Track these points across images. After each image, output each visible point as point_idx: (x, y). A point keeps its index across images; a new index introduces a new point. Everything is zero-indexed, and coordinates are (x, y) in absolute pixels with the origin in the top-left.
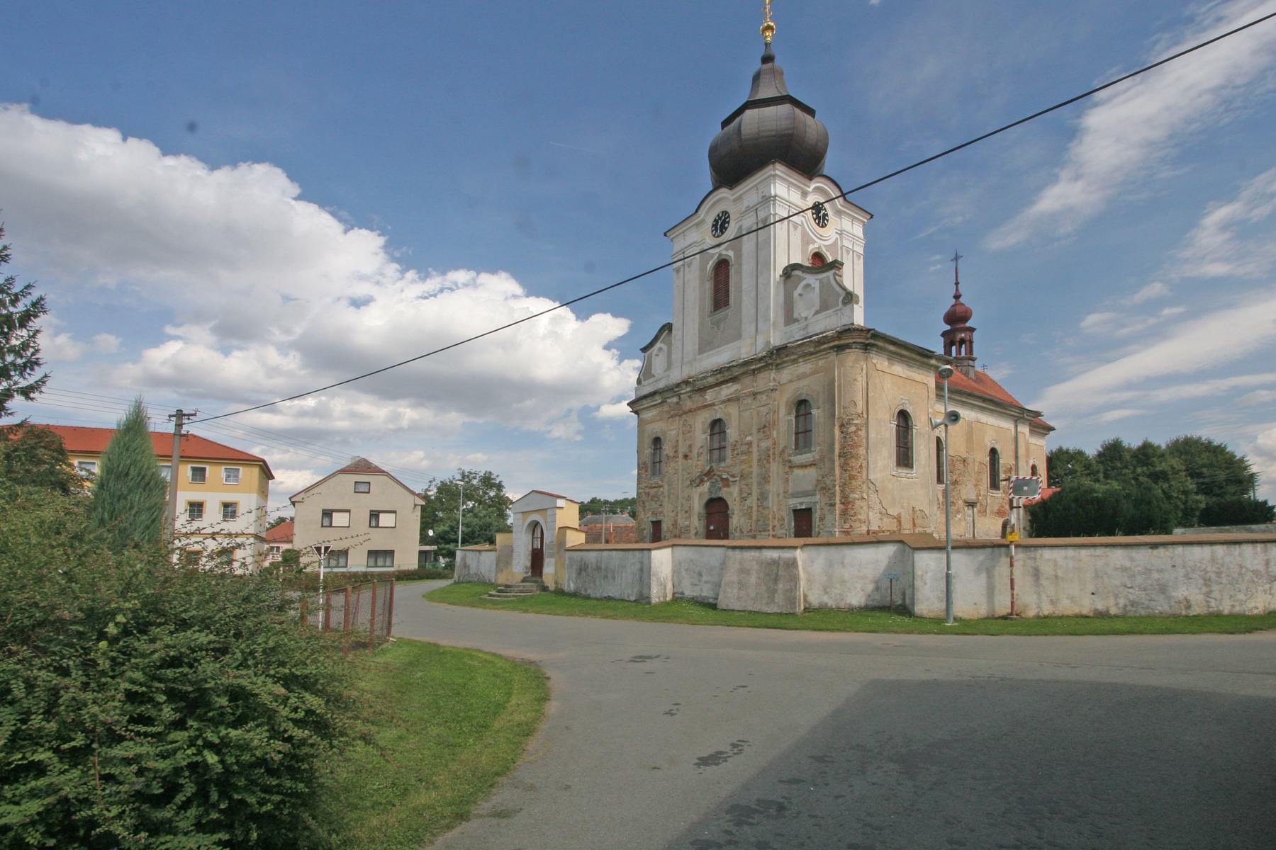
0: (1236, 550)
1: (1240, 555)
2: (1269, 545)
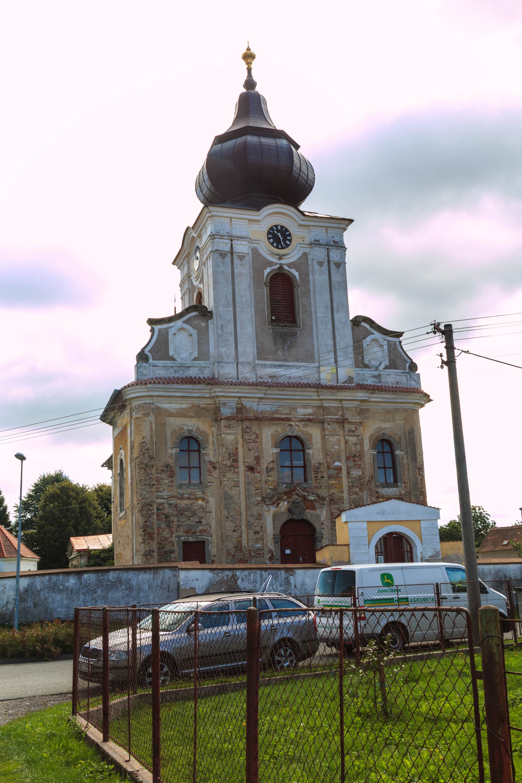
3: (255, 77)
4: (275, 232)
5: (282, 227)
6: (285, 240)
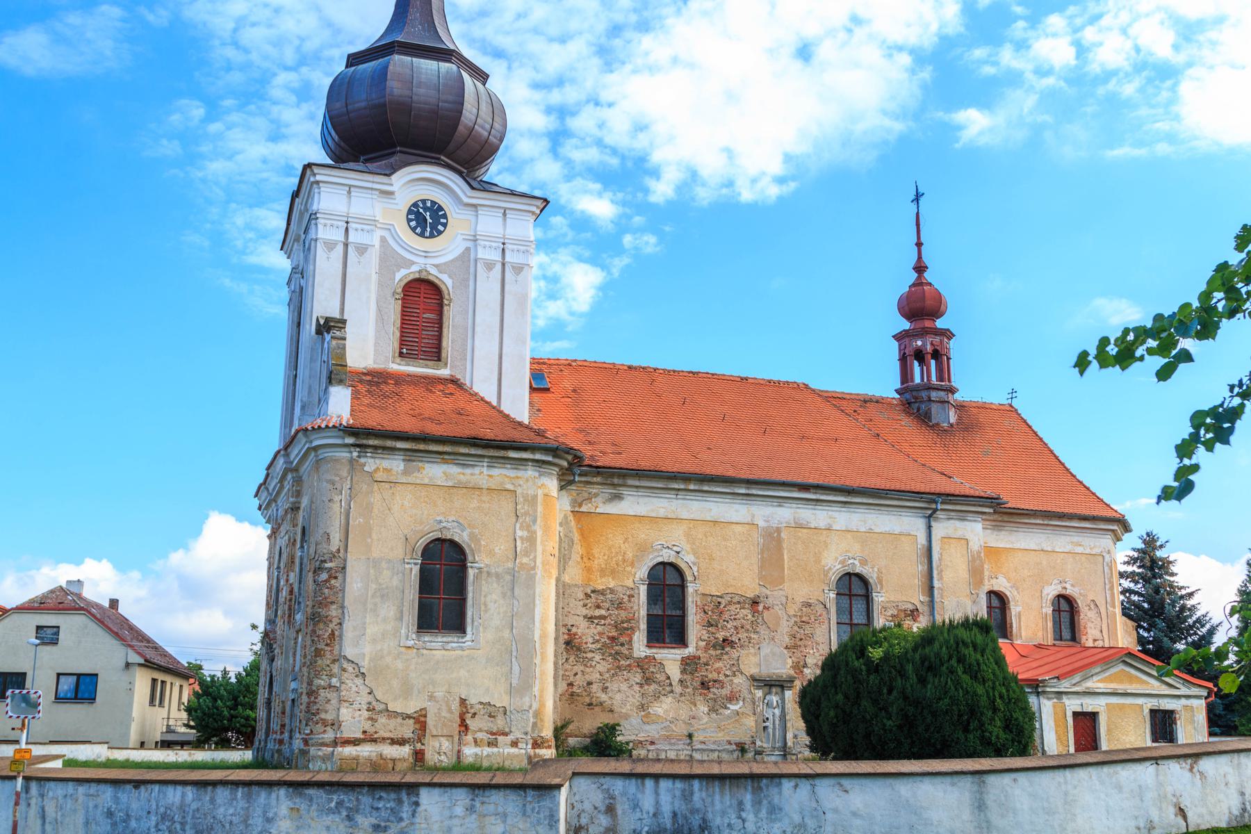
0: (208, 794)
1: (212, 801)
2: (255, 789)
5: (434, 203)
6: (434, 227)
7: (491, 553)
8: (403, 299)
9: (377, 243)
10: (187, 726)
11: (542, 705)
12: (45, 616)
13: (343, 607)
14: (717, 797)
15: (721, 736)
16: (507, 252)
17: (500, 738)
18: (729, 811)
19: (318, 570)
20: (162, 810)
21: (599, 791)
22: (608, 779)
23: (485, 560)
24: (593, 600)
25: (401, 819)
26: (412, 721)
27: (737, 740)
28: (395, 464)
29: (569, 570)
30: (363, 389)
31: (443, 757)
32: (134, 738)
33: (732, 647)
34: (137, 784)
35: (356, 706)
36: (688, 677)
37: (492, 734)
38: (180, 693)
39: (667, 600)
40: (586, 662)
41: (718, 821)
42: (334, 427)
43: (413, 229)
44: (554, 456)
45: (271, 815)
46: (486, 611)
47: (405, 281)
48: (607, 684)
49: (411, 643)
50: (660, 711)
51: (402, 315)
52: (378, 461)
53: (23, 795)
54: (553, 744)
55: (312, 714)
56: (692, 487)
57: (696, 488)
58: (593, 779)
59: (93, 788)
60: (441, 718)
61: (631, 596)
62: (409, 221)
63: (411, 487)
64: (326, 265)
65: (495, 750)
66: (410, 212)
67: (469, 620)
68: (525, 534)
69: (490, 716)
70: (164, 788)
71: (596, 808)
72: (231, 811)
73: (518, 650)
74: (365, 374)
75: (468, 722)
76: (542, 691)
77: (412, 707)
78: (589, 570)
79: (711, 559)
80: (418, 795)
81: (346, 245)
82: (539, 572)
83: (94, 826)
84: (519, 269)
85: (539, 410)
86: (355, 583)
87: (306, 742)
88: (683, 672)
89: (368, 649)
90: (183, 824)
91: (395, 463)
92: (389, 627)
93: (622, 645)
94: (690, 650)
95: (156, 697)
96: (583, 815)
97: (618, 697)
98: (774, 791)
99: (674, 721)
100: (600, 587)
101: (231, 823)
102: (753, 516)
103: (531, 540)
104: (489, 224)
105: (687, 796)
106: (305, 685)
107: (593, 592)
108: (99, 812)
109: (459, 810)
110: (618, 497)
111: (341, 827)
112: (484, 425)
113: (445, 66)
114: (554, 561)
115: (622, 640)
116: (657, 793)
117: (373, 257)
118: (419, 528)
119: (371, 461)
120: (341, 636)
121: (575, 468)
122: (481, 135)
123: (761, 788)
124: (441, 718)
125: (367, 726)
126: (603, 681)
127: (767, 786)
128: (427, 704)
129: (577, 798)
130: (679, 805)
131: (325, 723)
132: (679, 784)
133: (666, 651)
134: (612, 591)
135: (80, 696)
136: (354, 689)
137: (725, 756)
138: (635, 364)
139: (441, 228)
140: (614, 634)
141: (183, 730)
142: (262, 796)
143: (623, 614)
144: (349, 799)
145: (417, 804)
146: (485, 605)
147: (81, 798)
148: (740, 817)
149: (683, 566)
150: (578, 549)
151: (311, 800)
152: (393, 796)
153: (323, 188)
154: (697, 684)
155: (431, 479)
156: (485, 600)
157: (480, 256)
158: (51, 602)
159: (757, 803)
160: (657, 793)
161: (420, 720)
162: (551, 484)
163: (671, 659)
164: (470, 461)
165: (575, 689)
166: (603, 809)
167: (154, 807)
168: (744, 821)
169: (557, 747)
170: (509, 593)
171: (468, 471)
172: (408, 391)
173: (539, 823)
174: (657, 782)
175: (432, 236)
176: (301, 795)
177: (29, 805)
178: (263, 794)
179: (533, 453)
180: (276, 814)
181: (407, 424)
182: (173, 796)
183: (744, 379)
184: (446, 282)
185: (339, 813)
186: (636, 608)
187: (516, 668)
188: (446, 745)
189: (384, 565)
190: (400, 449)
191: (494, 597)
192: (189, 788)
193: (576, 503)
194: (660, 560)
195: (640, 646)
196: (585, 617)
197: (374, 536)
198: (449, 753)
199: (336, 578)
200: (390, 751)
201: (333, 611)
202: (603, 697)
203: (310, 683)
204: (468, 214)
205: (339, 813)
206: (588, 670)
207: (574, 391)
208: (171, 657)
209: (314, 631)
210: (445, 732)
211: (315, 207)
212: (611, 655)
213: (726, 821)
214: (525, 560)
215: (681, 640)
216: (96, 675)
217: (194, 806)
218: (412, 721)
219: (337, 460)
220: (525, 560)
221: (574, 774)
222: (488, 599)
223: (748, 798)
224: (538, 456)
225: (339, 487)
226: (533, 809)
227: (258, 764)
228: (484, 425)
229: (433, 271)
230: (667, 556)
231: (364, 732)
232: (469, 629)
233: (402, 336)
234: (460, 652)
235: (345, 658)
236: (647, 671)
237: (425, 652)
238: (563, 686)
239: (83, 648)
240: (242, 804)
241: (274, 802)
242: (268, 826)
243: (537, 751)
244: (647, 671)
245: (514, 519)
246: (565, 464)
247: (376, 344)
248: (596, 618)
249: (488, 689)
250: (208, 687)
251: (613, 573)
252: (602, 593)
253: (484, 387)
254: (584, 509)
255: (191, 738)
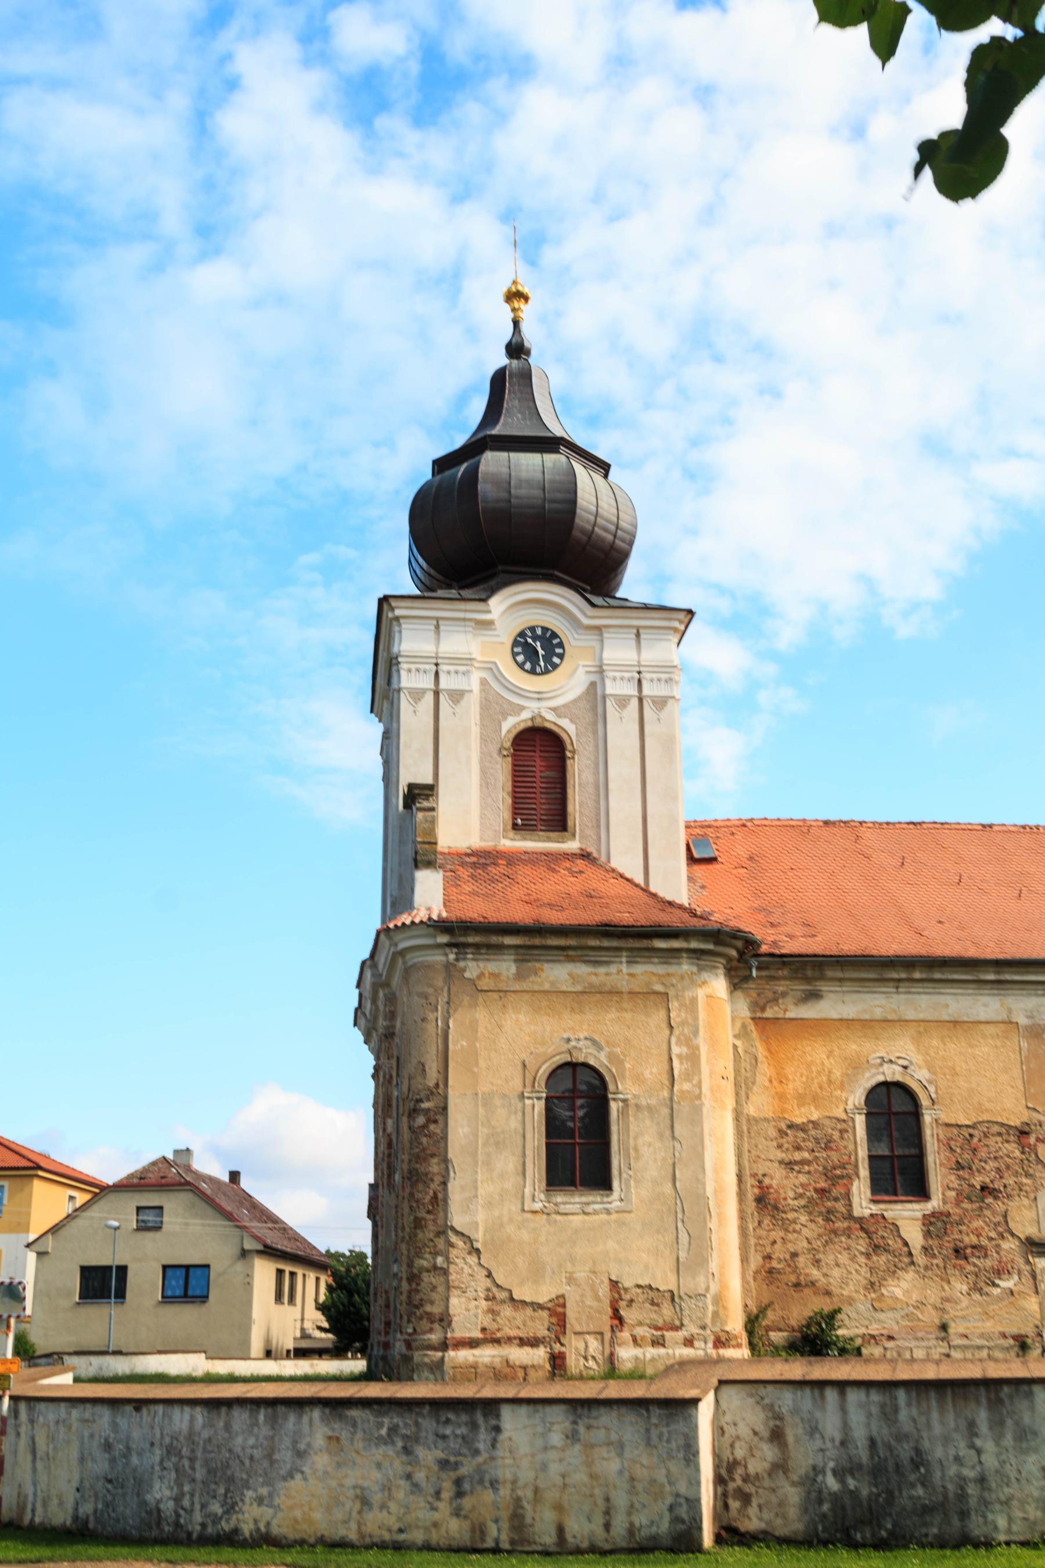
1: (228, 1427)
2: (281, 1409)
3: (530, 335)
4: (530, 640)
5: (545, 629)
6: (548, 659)
7: (639, 1079)
8: (514, 756)
9: (475, 686)
10: (321, 1329)
11: (724, 1286)
12: (147, 1195)
13: (446, 1161)
14: (935, 1415)
15: (990, 1326)
16: (645, 683)
17: (668, 1335)
18: (956, 1436)
19: (414, 1112)
20: (167, 1440)
21: (758, 1409)
22: (770, 1388)
23: (632, 1087)
24: (791, 1139)
25: (477, 1452)
26: (545, 1314)
27: (1015, 1331)
28: (506, 967)
29: (753, 1098)
30: (464, 873)
31: (591, 1363)
32: (257, 1346)
33: (996, 1198)
34: (139, 1404)
35: (471, 1294)
36: (934, 1243)
37: (657, 1328)
38: (313, 1287)
39: (895, 1134)
40: (786, 1226)
41: (939, 1452)
42: (422, 922)
43: (521, 666)
44: (716, 944)
45: (302, 1446)
46: (637, 1158)
47: (515, 732)
48: (821, 1256)
49: (538, 1206)
50: (898, 1292)
51: (514, 776)
52: (481, 964)
53: (11, 1422)
54: (744, 1339)
55: (414, 1305)
56: (917, 975)
57: (924, 976)
58: (747, 1387)
59: (88, 1411)
60: (586, 1309)
61: (842, 1132)
62: (514, 655)
63: (527, 997)
64: (414, 719)
65: (662, 1351)
66: (516, 643)
67: (615, 1172)
68: (684, 1050)
69: (653, 1303)
70: (169, 1409)
71: (755, 1433)
72: (251, 1441)
73: (685, 1210)
74: (467, 855)
75: (622, 1313)
76: (722, 1267)
77: (544, 1294)
78: (782, 1097)
79: (955, 1074)
80: (498, 1416)
81: (437, 693)
82: (707, 1101)
83: (90, 1464)
84: (661, 703)
85: (703, 887)
86: (460, 1129)
87: (409, 1345)
88: (927, 1234)
89: (481, 1217)
90: (192, 1460)
91: (504, 965)
92: (509, 1185)
93: (836, 1199)
94: (934, 1204)
95: (284, 1292)
96: (737, 1445)
97: (836, 1273)
98: (1022, 1405)
99: (921, 1305)
100: (799, 1121)
101: (252, 1458)
102: (1010, 1011)
103: (693, 1058)
104: (618, 651)
105: (889, 1414)
106: (404, 1268)
107: (789, 1127)
108: (95, 1444)
109: (556, 1438)
110: (815, 996)
111: (397, 1463)
112: (622, 908)
113: (550, 458)
114: (729, 1087)
115: (835, 1192)
116: (843, 1410)
117: (472, 705)
118: (541, 1050)
119: (471, 964)
120: (445, 1200)
121: (742, 956)
122: (603, 540)
123: (1000, 1401)
124: (586, 1309)
125: (487, 1321)
126: (812, 1250)
127: (1011, 1397)
128: (566, 1289)
129: (728, 1418)
130: (881, 1431)
131: (430, 1317)
132: (875, 1397)
133: (899, 1206)
134: (815, 1124)
135: (190, 1293)
136: (467, 1270)
137: (998, 1354)
138: (833, 818)
139: (556, 660)
140: (822, 1184)
141: (318, 1334)
142: (291, 1420)
143: (834, 1156)
144: (404, 1422)
145: (497, 1429)
146: (636, 1150)
147: (75, 1425)
148: (972, 1446)
149: (914, 1086)
150: (765, 1070)
151: (354, 1425)
152: (464, 1418)
153: (405, 625)
154: (948, 1251)
155: (552, 983)
156: (637, 1144)
157: (608, 691)
158: (152, 1178)
159: (997, 1424)
160: (843, 1410)
161: (557, 1313)
162: (718, 985)
163: (908, 1217)
164: (604, 957)
165: (775, 1264)
166: (766, 1433)
167: (158, 1436)
168: (979, 1452)
169: (752, 1346)
170: (668, 1133)
171: (602, 970)
172: (524, 873)
173: (670, 1456)
174: (842, 1394)
175: (546, 672)
176: (341, 1417)
177: (18, 1434)
178: (292, 1418)
179: (687, 940)
180: (309, 1445)
181: (520, 914)
182: (181, 1420)
183: (987, 827)
184: (568, 727)
185: (393, 1443)
186: (851, 1147)
187: (684, 1238)
188: (594, 1344)
189: (498, 1102)
190: (510, 947)
191: (648, 1138)
192: (198, 1409)
193: (758, 1006)
194: (881, 1078)
195: (862, 1198)
196: (781, 1162)
197: (482, 1063)
198: (599, 1357)
199: (436, 1122)
200: (520, 1355)
201: (434, 1167)
202: (815, 1274)
203: (410, 1265)
204: (590, 640)
205: (393, 1443)
206: (790, 1236)
207: (751, 858)
208: (304, 1241)
209: (412, 1195)
210: (592, 1328)
211: (395, 650)
212: (820, 1214)
213: (952, 1452)
214: (686, 1086)
215: (920, 1190)
216: (208, 1266)
217: (206, 1434)
218: (545, 1314)
219: (429, 967)
220: (686, 1086)
221: (721, 1382)
222: (640, 1141)
223: (982, 1416)
224: (694, 944)
225: (433, 1002)
226: (660, 1437)
227: (368, 1377)
228: (622, 908)
229: (550, 716)
230: (892, 1073)
231: (484, 1330)
232: (616, 1184)
233: (514, 803)
234: (604, 1217)
235: (453, 1229)
236: (876, 1236)
237: (558, 1218)
238: (756, 1260)
239: (189, 1234)
240: (265, 1431)
241: (306, 1428)
242: (298, 1461)
243: (722, 1351)
244: (876, 1236)
245: (668, 1032)
246: (734, 953)
247: (483, 816)
248: (796, 1163)
249: (646, 1267)
250: (341, 1278)
251: (816, 1100)
252: (802, 1128)
253: (625, 859)
254: (769, 1013)
255: (330, 1345)
